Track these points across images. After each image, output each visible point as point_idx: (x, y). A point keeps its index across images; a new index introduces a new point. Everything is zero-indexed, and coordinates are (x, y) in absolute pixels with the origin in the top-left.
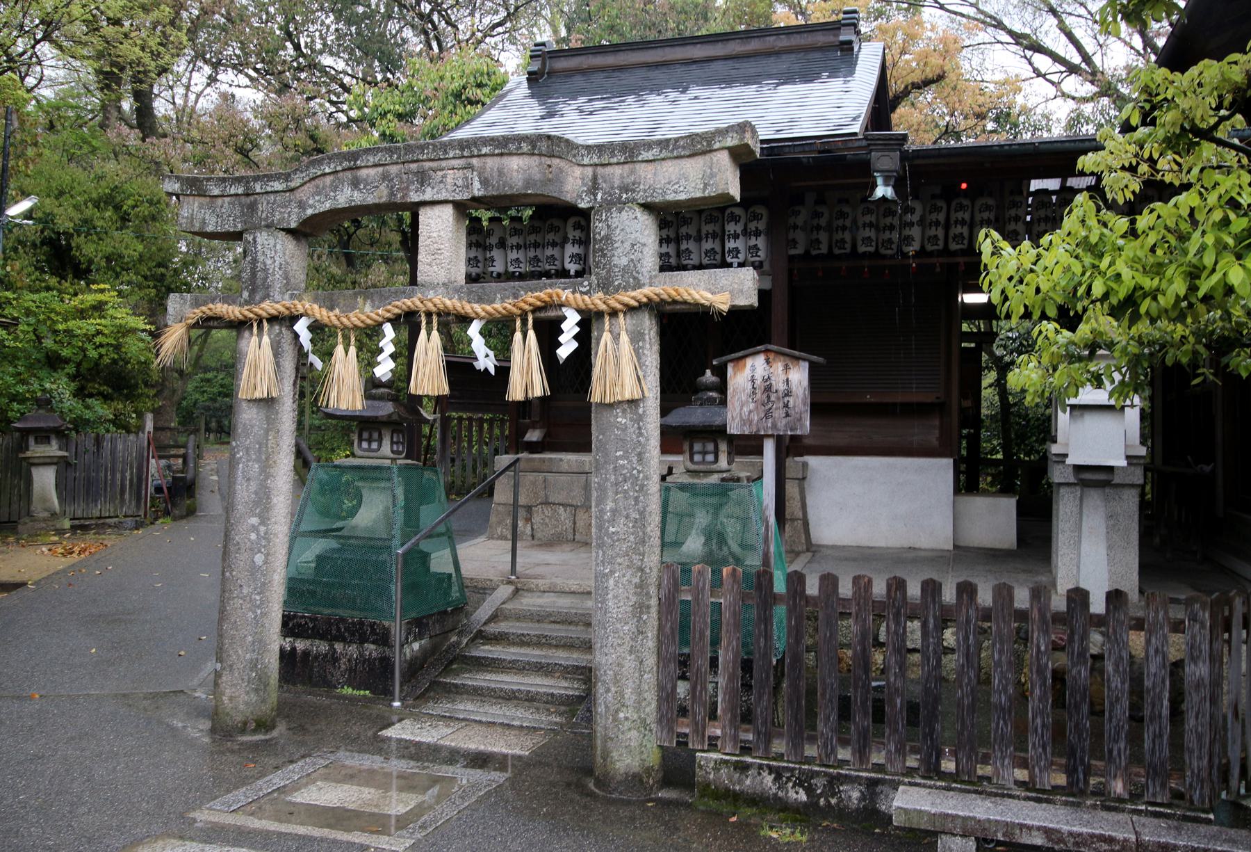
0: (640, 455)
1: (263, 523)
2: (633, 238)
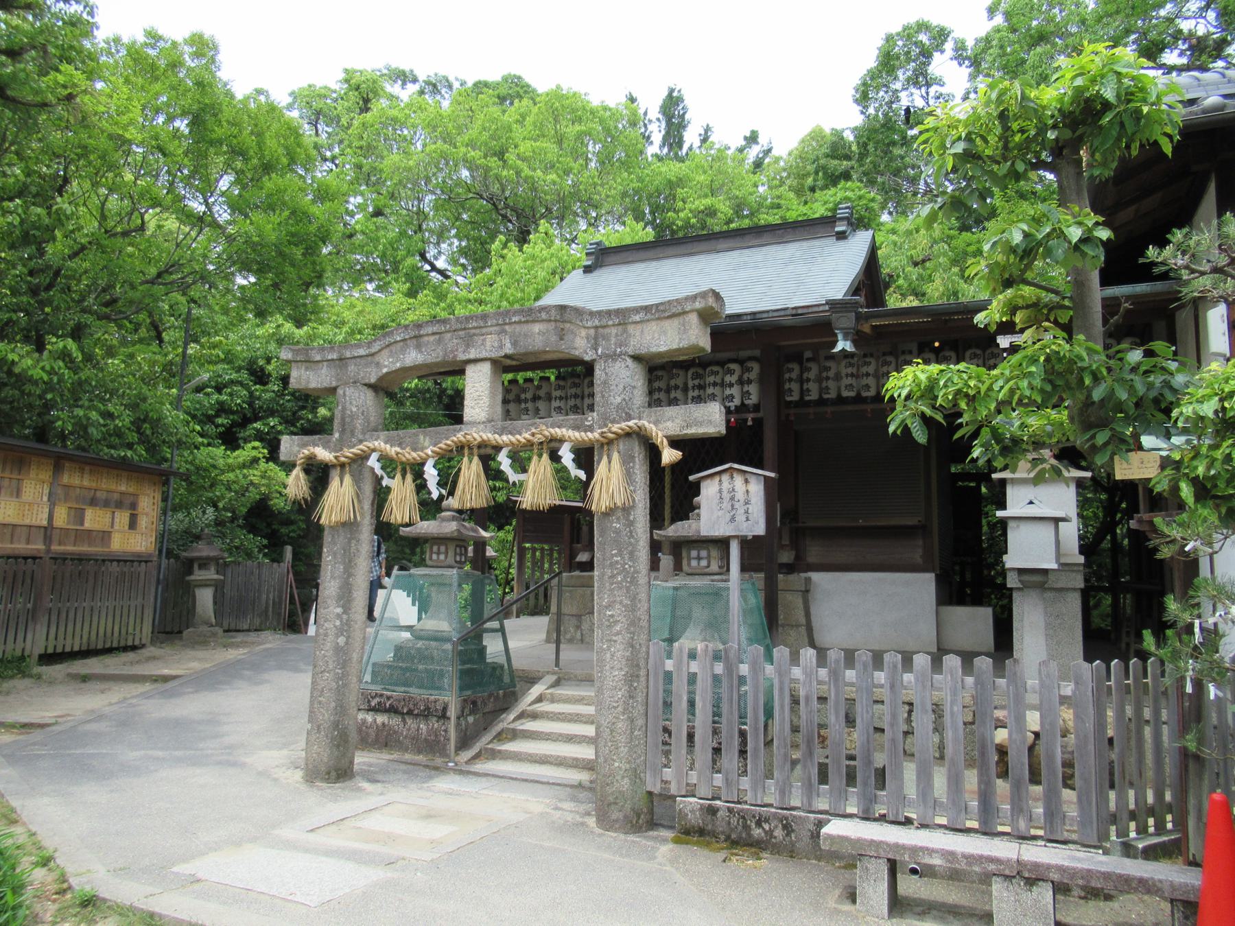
0: (631, 553)
1: (345, 612)
2: (620, 382)
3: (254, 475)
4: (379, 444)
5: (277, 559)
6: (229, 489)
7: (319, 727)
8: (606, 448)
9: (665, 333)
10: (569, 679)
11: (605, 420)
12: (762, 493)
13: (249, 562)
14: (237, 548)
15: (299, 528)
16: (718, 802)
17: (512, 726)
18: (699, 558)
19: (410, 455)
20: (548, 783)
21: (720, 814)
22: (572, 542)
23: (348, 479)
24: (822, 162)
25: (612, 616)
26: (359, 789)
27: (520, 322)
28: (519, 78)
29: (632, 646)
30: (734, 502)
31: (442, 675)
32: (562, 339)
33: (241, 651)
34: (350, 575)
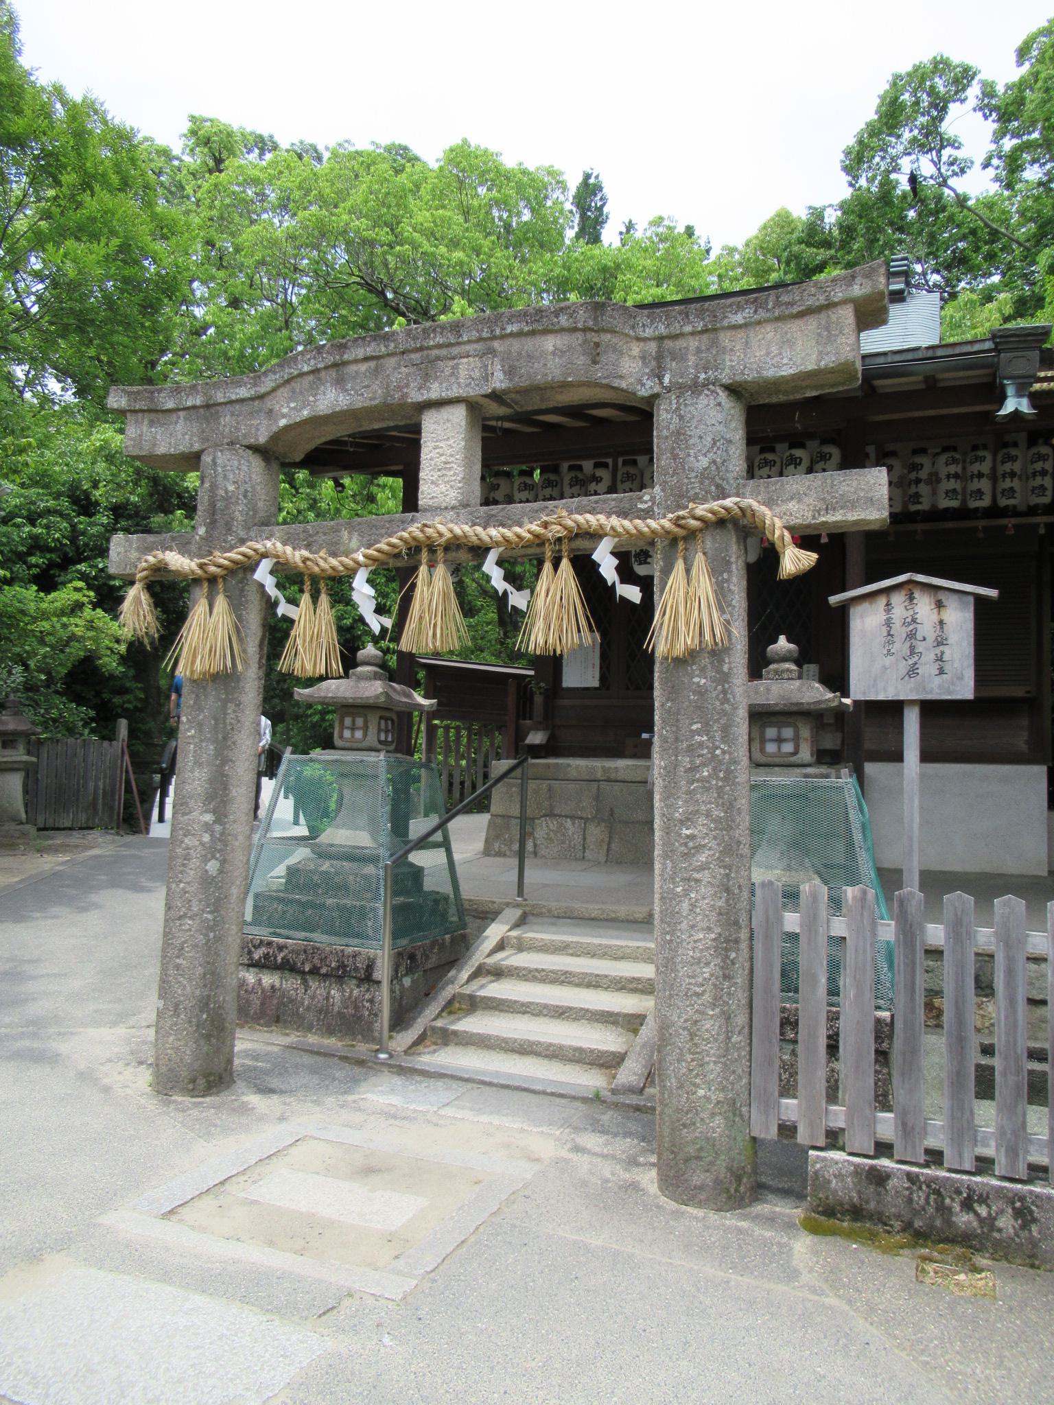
0: (726, 729)
1: (218, 821)
2: (702, 432)
3: (77, 625)
4: (273, 545)
5: (110, 737)
6: (42, 642)
7: (177, 1006)
8: (681, 545)
9: (790, 343)
10: (540, 915)
11: (680, 498)
12: (970, 625)
13: (71, 740)
14: (54, 720)
15: (136, 699)
16: (885, 1163)
17: (467, 990)
18: (779, 740)
19: (326, 562)
20: (544, 1093)
21: (891, 1183)
22: (518, 717)
23: (221, 603)
24: (795, 248)
25: (692, 837)
26: (245, 1109)
27: (520, 334)
28: (405, 149)
29: (728, 890)
30: (916, 641)
31: (363, 914)
32: (595, 362)
33: (63, 858)
34: (225, 761)
